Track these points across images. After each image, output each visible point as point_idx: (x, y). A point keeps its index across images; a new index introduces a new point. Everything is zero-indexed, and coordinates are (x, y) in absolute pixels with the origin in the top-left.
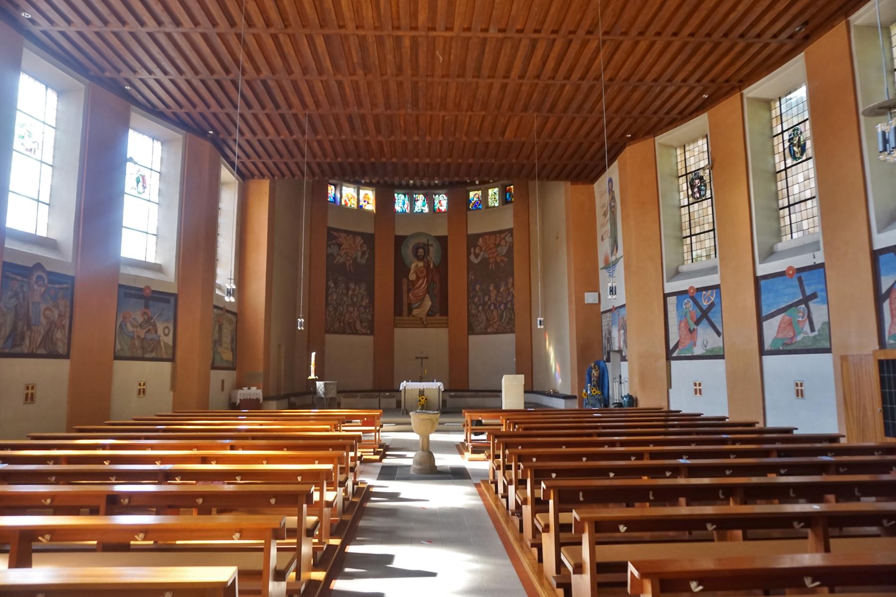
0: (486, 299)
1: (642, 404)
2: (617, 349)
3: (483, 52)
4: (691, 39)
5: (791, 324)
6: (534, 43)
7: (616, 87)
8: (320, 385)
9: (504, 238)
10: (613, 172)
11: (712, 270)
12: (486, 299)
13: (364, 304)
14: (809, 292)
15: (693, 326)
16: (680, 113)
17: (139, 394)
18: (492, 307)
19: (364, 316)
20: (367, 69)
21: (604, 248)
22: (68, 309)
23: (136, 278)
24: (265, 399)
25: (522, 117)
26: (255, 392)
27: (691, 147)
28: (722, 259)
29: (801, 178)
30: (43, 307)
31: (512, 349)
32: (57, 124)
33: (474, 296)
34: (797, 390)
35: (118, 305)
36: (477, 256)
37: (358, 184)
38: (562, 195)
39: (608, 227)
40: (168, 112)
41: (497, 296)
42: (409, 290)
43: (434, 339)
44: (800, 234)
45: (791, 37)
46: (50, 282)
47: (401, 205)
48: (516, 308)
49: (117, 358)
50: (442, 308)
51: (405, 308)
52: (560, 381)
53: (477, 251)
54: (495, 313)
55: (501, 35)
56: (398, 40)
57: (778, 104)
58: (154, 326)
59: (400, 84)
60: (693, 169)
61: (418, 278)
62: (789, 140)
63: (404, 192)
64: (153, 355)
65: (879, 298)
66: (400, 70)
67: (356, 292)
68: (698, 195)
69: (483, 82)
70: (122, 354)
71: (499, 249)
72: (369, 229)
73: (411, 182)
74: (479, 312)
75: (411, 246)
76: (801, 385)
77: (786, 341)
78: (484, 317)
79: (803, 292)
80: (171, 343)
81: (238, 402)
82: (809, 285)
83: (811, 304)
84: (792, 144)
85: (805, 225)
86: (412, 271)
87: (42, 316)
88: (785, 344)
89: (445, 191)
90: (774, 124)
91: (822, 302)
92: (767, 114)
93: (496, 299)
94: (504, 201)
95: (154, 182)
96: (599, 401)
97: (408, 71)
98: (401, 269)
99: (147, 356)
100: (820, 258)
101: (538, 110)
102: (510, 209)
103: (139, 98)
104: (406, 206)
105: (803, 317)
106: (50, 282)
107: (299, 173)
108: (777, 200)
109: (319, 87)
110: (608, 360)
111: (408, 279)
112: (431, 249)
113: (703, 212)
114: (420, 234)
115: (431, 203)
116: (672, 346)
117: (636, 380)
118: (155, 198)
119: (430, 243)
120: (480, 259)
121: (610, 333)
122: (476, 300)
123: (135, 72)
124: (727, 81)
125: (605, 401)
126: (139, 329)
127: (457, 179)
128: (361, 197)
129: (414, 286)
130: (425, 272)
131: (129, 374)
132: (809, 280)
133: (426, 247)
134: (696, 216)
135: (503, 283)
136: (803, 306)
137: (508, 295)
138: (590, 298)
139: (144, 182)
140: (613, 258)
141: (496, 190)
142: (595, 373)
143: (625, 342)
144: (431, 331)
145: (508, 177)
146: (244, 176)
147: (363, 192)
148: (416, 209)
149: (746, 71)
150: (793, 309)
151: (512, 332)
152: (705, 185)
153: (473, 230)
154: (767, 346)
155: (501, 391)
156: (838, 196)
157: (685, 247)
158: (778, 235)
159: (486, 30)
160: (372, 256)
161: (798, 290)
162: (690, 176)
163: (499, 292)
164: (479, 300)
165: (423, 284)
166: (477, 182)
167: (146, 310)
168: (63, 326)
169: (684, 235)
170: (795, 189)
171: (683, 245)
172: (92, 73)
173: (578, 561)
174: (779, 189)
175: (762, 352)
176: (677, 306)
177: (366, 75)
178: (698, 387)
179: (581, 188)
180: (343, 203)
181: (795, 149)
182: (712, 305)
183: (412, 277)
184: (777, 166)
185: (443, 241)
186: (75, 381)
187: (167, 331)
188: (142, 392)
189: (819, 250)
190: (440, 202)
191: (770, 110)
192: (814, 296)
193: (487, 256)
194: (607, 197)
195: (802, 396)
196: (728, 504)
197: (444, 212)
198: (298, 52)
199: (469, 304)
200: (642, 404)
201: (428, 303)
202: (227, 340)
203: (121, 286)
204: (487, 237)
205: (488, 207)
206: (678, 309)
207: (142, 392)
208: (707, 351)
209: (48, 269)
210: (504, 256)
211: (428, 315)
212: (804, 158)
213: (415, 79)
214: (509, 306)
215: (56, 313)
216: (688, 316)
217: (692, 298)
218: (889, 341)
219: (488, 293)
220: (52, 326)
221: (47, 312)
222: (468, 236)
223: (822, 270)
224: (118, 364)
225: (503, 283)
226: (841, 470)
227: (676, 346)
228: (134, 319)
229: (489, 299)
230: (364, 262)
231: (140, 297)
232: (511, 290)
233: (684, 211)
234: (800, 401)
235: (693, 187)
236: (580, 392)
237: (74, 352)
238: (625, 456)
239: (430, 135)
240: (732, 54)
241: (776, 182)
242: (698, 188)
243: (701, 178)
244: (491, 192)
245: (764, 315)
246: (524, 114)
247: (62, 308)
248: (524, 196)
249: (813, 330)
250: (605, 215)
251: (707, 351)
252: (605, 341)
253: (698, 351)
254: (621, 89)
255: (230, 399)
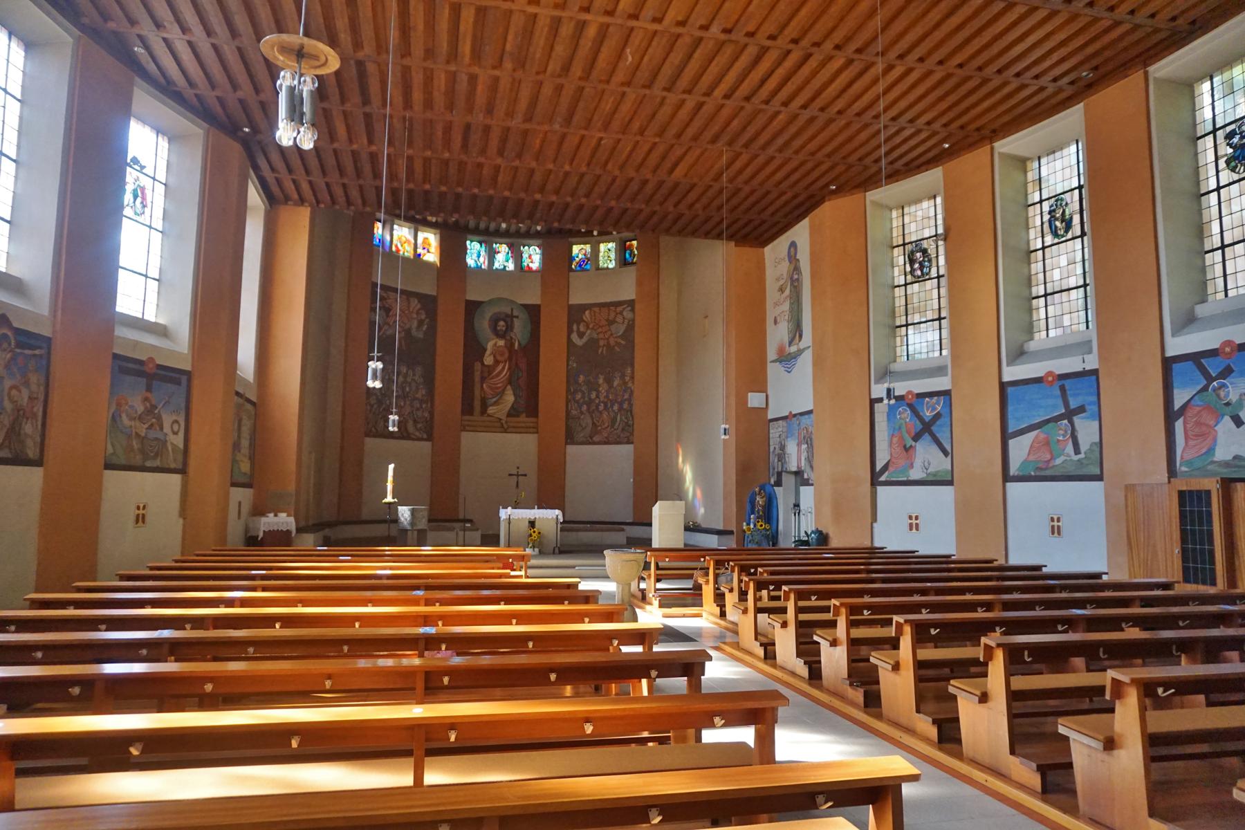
0: (593, 395)
1: (835, 543)
2: (794, 469)
3: (690, 56)
4: (959, 71)
5: (1047, 443)
6: (764, 50)
7: (843, 122)
8: (404, 512)
9: (621, 313)
10: (801, 233)
11: (939, 371)
12: (593, 395)
13: (419, 395)
14: (1073, 404)
15: (910, 442)
16: (907, 164)
17: (137, 522)
18: (601, 407)
19: (419, 413)
20: (521, 63)
21: (777, 335)
22: (42, 388)
23: (136, 344)
24: (299, 530)
25: (706, 150)
26: (284, 521)
27: (913, 208)
28: (955, 356)
29: (1063, 261)
30: (8, 383)
31: (628, 467)
32: (23, 94)
33: (576, 391)
34: (1053, 527)
35: (112, 385)
36: (581, 335)
37: (418, 222)
38: (715, 261)
39: (786, 307)
40: (189, 93)
41: (607, 392)
42: (483, 379)
43: (519, 448)
44: (1060, 331)
45: (1072, 83)
46: (19, 345)
47: (475, 257)
48: (636, 409)
49: (109, 466)
50: (529, 406)
51: (477, 404)
52: (702, 511)
53: (582, 329)
54: (605, 415)
55: (723, 37)
56: (581, 26)
57: (1036, 164)
58: (159, 418)
59: (559, 89)
60: (914, 239)
61: (497, 362)
62: (1050, 213)
63: (481, 238)
64: (157, 463)
65: (1170, 416)
66: (566, 68)
67: (409, 380)
68: (919, 273)
69: (672, 98)
70: (115, 461)
71: (613, 328)
72: (428, 289)
73: (504, 225)
74: (582, 413)
75: (488, 315)
76: (1058, 520)
77: (1040, 465)
78: (590, 422)
79: (1066, 404)
80: (181, 446)
81: (261, 535)
82: (1075, 395)
83: (1076, 420)
84: (1053, 217)
85: (1066, 320)
86: (488, 352)
87: (6, 398)
88: (1039, 469)
89: (539, 242)
90: (1030, 190)
91: (1092, 417)
92: (1020, 176)
93: (607, 397)
94: (623, 262)
95: (157, 198)
96: (767, 537)
97: (577, 70)
98: (473, 349)
99: (148, 464)
100: (1092, 362)
101: (730, 143)
102: (631, 272)
103: (151, 67)
104: (482, 259)
105: (1064, 436)
106: (19, 345)
107: (360, 201)
108: (1030, 286)
109: (441, 81)
110: (779, 483)
111: (483, 364)
112: (517, 323)
113: (928, 295)
114: (500, 300)
115: (518, 257)
116: (878, 468)
117: (827, 510)
118: (158, 223)
119: (515, 313)
120: (585, 339)
121: (783, 448)
122: (579, 396)
123: (159, 25)
124: (978, 129)
125: (774, 538)
126: (138, 423)
127: (569, 226)
128: (420, 241)
129: (490, 373)
130: (507, 355)
131: (126, 490)
132: (1075, 392)
133: (509, 319)
134: (915, 300)
135: (617, 375)
136: (1066, 421)
137: (625, 391)
138: (755, 400)
139: (144, 198)
140: (793, 349)
141: (612, 245)
142: (760, 500)
143: (810, 460)
144: (513, 439)
145: (628, 227)
146: (272, 200)
147: (421, 236)
148: (496, 265)
149: (1006, 118)
150: (1051, 425)
151: (629, 442)
152: (930, 261)
153: (576, 299)
154: (1013, 470)
155: (650, 525)
156: (1109, 287)
157: (898, 339)
158: (1030, 330)
159: (705, 28)
160: (432, 331)
161: (1060, 402)
162: (909, 248)
163: (611, 386)
164: (583, 397)
165: (503, 371)
166: (595, 233)
167: (148, 395)
168: (35, 415)
169: (898, 323)
170: (1056, 275)
171: (895, 337)
172: (85, 20)
173: (1109, 734)
174: (1033, 272)
175: (1006, 478)
176: (888, 415)
177: (514, 70)
178: (914, 522)
179: (748, 252)
180: (394, 249)
181: (1058, 224)
182: (938, 416)
183: (488, 360)
184: (1032, 243)
185: (533, 312)
186: (50, 498)
187: (176, 427)
188: (140, 519)
189: (1090, 352)
190: (530, 257)
191: (1025, 172)
192: (1081, 409)
193: (595, 336)
194: (785, 267)
195: (1059, 533)
196: (1179, 664)
197: (536, 271)
198: (430, 25)
199: (568, 401)
200: (835, 543)
201: (510, 398)
202: (245, 443)
203: (116, 356)
204: (596, 309)
205: (598, 269)
206: (889, 420)
207: (140, 519)
208: (928, 475)
209: (16, 325)
210: (621, 337)
211: (509, 415)
212: (1069, 236)
213: (582, 83)
214: (625, 406)
215: (25, 393)
216: (904, 430)
217: (910, 406)
218: (1181, 468)
219: (593, 386)
220: (20, 414)
221: (14, 392)
222: (570, 307)
223: (1094, 378)
224: (108, 474)
225: (617, 375)
226: (1181, 624)
227: (886, 468)
228: (132, 407)
229: (597, 397)
230: (421, 335)
231: (140, 374)
232: (630, 385)
233: (899, 292)
234: (1055, 539)
235: (912, 262)
236: (739, 524)
237: (50, 454)
238: (1029, 605)
239: (571, 164)
240: (998, 96)
241: (1029, 264)
242: (920, 263)
243: (924, 251)
244: (603, 247)
245: (1010, 431)
246: (709, 146)
247: (34, 387)
248: (652, 254)
249: (1077, 451)
250: (781, 290)
251: (928, 475)
252: (774, 459)
253: (916, 474)
254: (848, 124)
255: (247, 530)
